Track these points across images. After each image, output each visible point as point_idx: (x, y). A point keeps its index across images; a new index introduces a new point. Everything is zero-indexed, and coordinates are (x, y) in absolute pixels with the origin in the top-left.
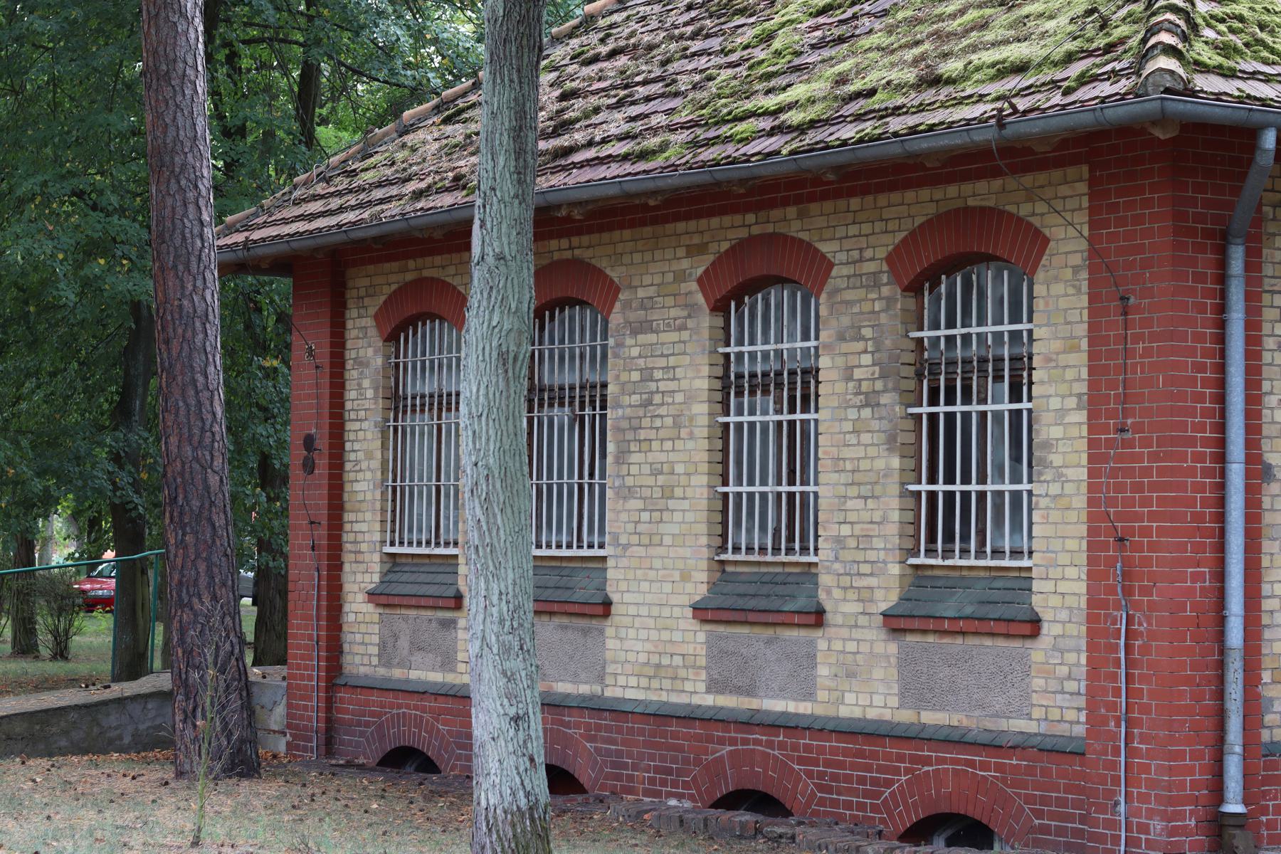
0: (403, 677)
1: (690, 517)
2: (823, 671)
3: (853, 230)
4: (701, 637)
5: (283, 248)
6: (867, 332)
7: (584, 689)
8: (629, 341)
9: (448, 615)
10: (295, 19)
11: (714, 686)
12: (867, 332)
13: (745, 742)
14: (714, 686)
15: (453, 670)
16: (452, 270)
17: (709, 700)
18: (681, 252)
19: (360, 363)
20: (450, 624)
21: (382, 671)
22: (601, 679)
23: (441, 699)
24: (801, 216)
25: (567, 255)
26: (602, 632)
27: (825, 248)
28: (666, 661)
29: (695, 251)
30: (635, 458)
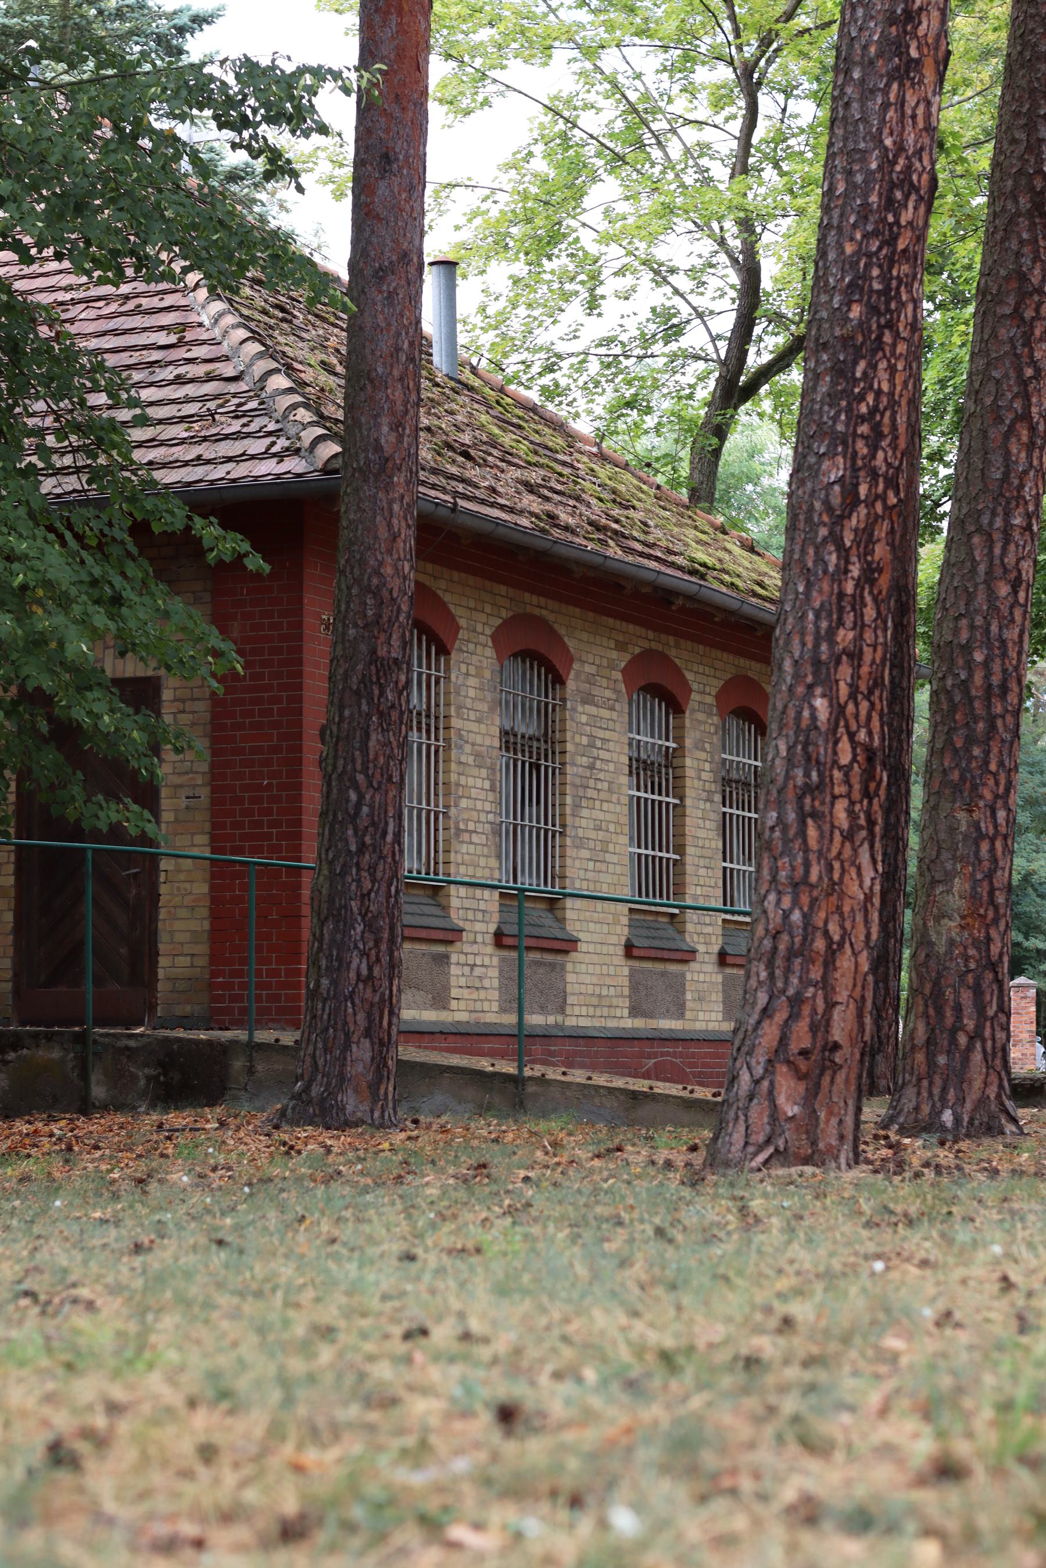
0: (556, 1025)
1: (618, 869)
2: (689, 996)
3: (701, 669)
4: (626, 971)
5: (489, 527)
6: (707, 746)
7: (551, 1020)
8: (580, 709)
9: (440, 949)
10: (107, 159)
11: (635, 1011)
12: (707, 746)
13: (663, 1054)
14: (635, 1011)
15: (445, 1007)
16: (443, 584)
17: (629, 1023)
18: (612, 644)
19: (922, 745)
20: (443, 960)
21: (639, 1023)
22: (562, 1010)
23: (451, 1038)
24: (677, 646)
25: (537, 612)
26: (563, 967)
27: (689, 676)
28: (605, 992)
29: (621, 647)
30: (585, 813)
